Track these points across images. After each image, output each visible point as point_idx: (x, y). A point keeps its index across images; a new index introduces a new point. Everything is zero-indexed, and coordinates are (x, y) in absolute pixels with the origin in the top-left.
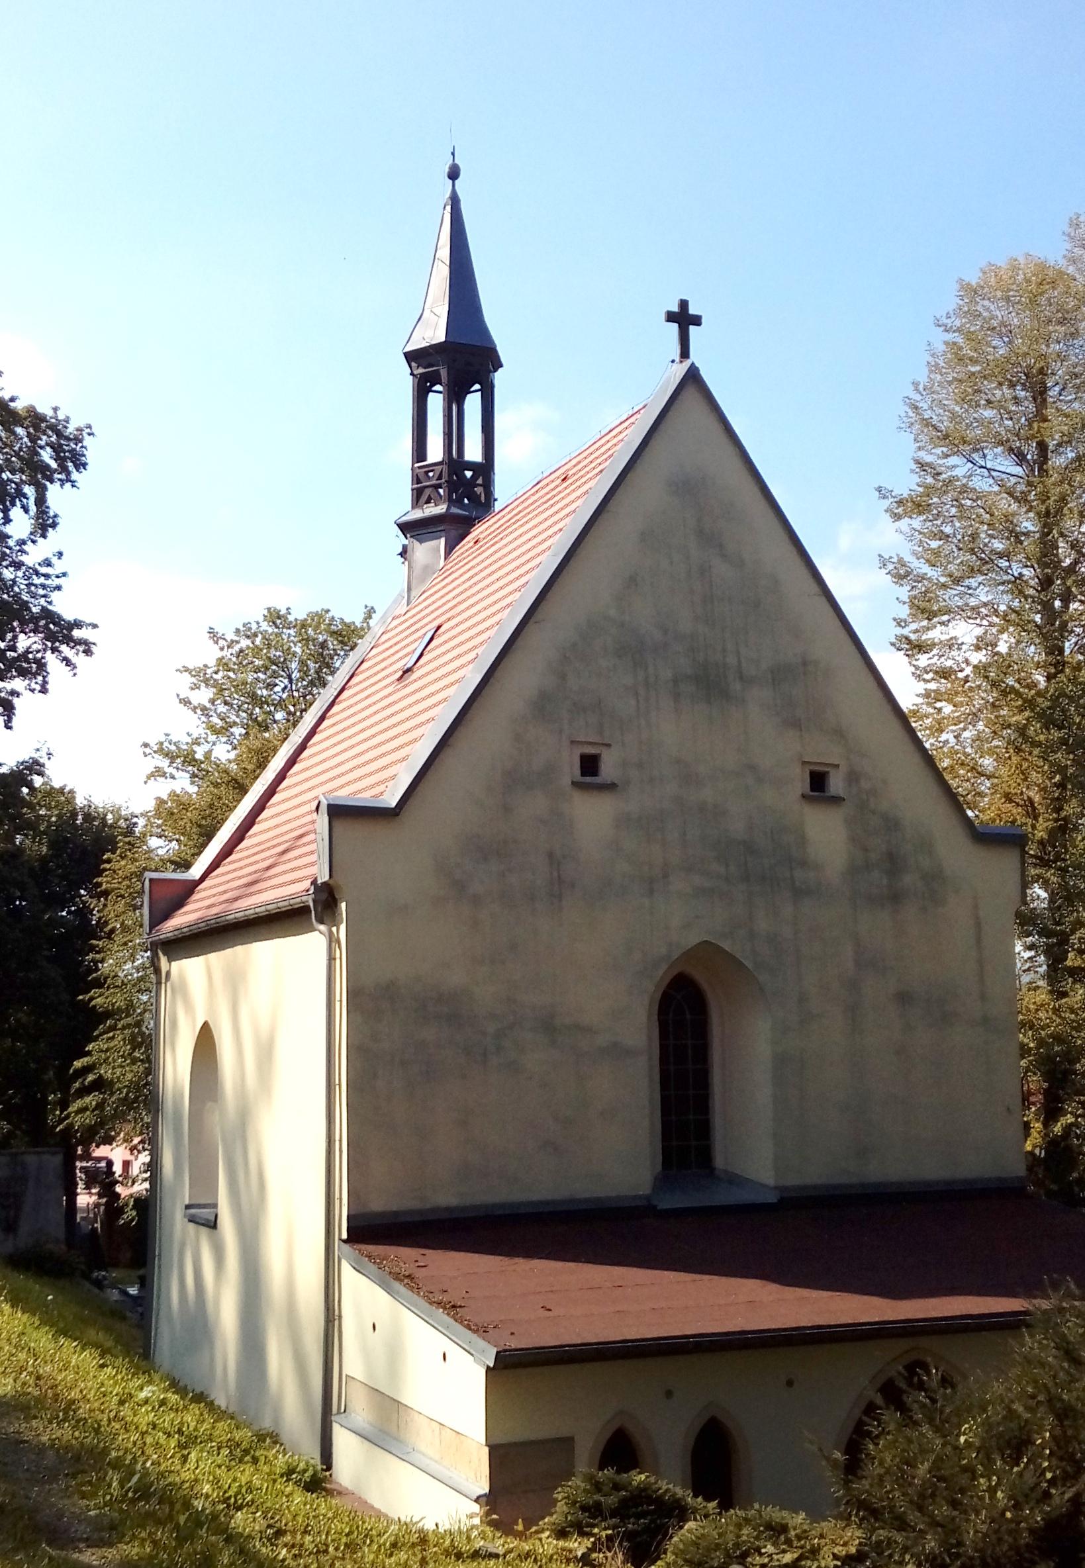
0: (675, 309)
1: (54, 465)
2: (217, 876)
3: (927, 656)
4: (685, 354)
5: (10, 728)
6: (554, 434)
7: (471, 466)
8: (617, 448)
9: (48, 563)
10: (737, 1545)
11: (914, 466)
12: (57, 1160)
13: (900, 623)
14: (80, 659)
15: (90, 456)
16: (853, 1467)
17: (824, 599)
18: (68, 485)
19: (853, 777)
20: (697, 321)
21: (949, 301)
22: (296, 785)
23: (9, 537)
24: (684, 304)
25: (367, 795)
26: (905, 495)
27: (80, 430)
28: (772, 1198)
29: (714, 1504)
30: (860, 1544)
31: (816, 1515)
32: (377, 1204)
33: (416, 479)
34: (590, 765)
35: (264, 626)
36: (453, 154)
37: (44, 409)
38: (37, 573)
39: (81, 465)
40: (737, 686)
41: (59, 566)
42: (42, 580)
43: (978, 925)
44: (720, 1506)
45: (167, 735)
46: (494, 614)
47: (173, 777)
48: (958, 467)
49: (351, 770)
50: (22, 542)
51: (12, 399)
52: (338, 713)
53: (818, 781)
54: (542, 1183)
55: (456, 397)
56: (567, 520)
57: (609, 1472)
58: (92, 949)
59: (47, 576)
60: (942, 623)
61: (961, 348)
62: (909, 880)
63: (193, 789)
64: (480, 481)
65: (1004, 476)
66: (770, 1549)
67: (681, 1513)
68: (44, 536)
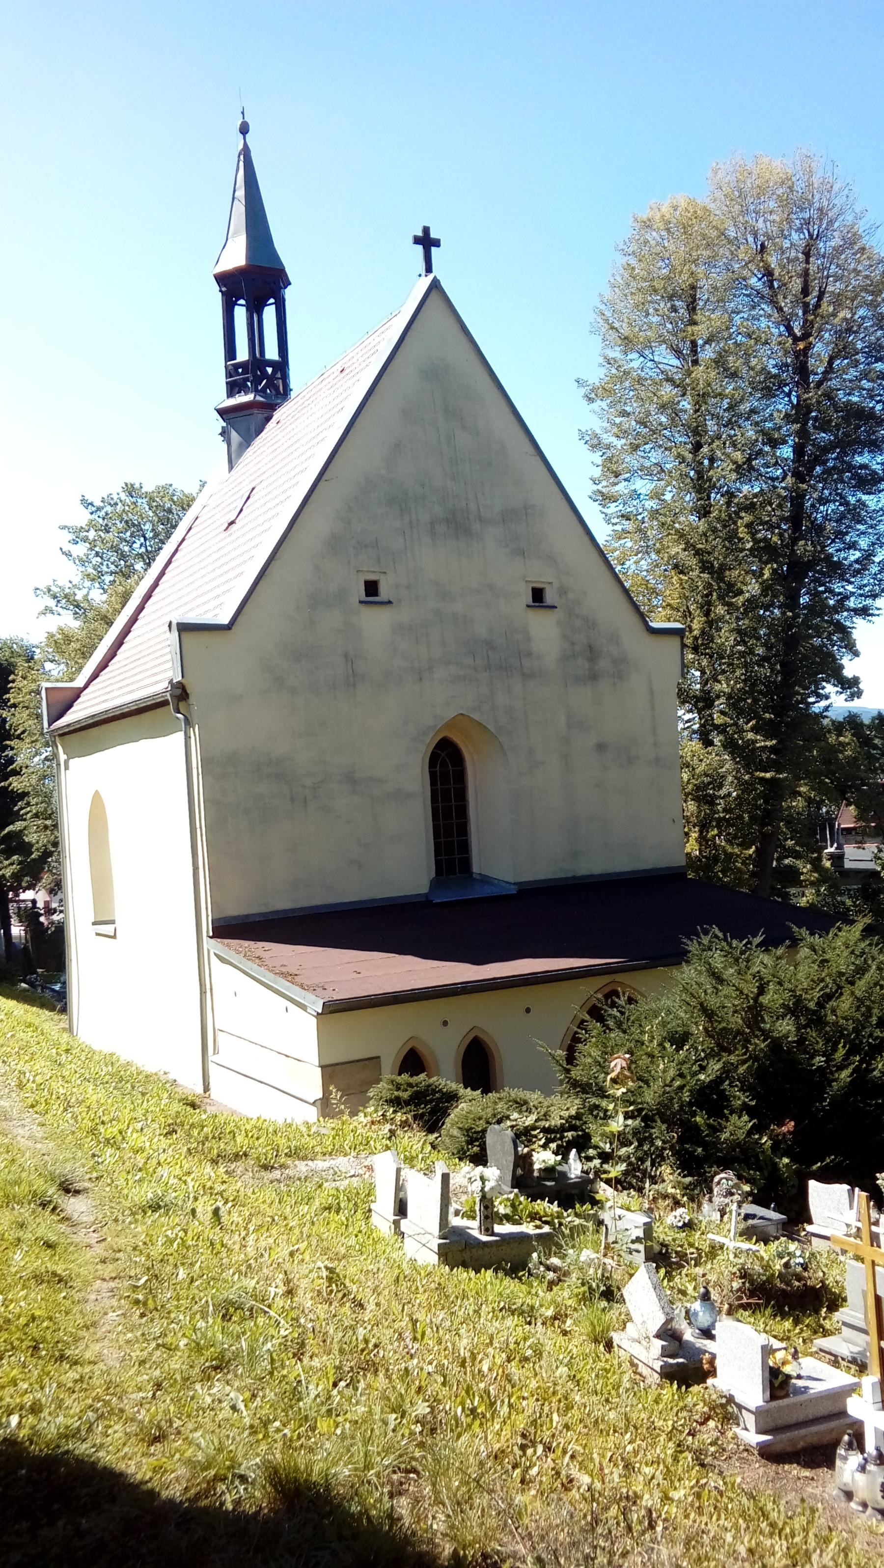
0: (420, 233)
3: (615, 504)
4: (429, 269)
7: (271, 363)
10: (494, 1115)
11: (601, 360)
13: (595, 481)
16: (571, 1059)
17: (538, 458)
19: (563, 591)
20: (437, 243)
21: (626, 230)
24: (426, 230)
26: (597, 384)
28: (513, 890)
29: (479, 1092)
31: (548, 1093)
32: (235, 909)
33: (229, 374)
34: (372, 588)
35: (123, 496)
40: (476, 526)
43: (652, 693)
48: (635, 362)
53: (538, 595)
57: (405, 1077)
60: (625, 480)
61: (633, 269)
62: (603, 664)
64: (279, 375)
65: (668, 367)
66: (515, 1115)
67: (452, 1098)
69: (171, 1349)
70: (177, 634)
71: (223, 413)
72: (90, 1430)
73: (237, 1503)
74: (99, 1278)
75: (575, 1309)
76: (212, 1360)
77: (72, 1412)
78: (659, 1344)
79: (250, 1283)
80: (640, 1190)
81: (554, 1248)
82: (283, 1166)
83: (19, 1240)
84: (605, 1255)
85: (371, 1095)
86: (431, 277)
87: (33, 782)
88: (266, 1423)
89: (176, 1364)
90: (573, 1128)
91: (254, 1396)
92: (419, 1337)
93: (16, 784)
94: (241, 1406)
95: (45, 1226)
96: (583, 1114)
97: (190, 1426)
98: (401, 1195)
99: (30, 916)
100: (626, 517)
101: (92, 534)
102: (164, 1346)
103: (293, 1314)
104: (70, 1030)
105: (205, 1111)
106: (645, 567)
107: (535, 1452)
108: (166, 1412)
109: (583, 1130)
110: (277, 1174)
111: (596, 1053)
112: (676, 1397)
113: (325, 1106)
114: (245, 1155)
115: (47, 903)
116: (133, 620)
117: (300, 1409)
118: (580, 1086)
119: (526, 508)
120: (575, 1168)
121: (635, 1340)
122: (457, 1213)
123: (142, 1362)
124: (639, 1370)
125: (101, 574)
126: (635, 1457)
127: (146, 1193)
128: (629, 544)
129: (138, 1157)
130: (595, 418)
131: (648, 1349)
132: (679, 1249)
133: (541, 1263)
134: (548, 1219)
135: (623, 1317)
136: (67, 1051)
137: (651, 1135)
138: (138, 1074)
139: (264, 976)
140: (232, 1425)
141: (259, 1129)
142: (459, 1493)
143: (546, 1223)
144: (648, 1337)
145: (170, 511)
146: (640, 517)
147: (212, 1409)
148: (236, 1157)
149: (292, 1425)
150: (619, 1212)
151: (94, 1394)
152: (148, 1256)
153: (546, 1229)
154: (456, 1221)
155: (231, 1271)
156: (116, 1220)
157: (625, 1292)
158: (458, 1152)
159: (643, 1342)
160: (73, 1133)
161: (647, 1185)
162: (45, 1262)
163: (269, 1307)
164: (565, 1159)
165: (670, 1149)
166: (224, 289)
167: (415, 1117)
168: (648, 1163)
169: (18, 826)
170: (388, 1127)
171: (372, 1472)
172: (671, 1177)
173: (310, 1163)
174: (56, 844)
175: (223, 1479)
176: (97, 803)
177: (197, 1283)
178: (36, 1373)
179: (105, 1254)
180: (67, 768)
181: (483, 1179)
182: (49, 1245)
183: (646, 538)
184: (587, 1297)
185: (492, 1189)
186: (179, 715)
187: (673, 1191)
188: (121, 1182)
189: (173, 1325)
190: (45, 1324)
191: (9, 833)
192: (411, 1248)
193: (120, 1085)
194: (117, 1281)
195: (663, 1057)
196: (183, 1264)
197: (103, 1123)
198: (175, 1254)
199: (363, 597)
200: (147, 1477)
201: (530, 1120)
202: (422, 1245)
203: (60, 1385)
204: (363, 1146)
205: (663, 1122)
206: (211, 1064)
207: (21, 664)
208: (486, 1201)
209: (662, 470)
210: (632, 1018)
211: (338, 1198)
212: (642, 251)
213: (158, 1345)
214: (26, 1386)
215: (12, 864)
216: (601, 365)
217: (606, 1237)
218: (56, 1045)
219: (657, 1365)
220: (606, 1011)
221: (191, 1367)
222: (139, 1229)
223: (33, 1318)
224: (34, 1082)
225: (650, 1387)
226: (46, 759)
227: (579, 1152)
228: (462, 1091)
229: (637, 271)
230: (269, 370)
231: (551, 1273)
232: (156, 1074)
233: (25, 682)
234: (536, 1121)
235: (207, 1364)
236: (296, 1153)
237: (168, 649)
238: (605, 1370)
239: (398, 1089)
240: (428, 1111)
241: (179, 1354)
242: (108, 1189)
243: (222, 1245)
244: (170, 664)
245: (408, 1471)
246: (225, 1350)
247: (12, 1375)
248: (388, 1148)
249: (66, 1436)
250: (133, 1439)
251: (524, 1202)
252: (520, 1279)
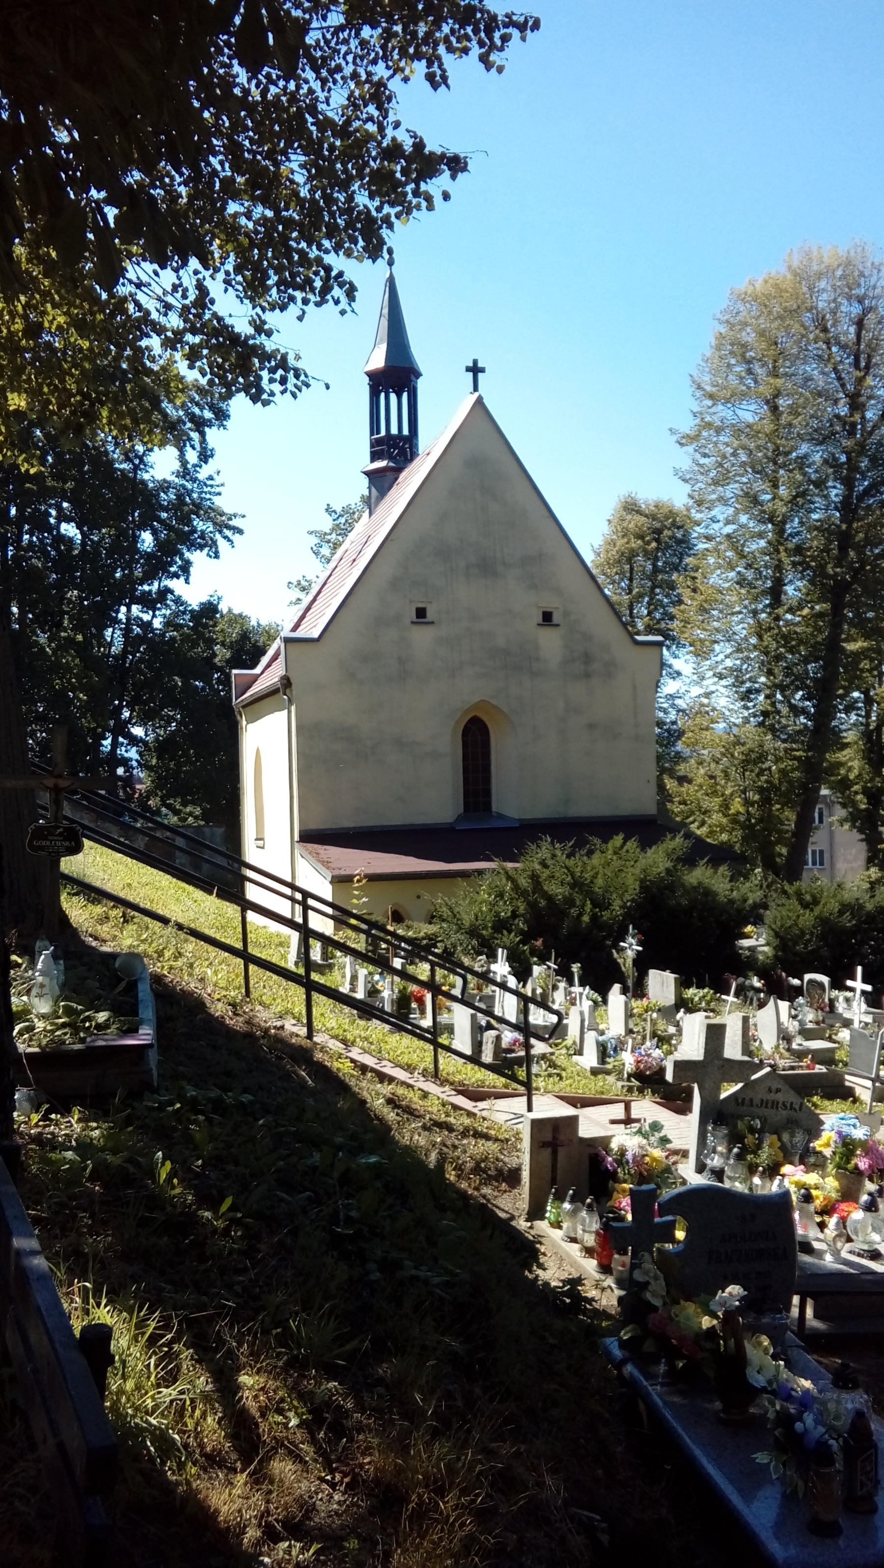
0: (471, 365)
4: (476, 389)
6: (439, 421)
9: (211, 478)
14: (236, 538)
19: (566, 614)
20: (482, 370)
24: (475, 362)
32: (313, 826)
33: (372, 446)
34: (421, 613)
38: (206, 486)
43: (635, 688)
50: (195, 466)
53: (547, 617)
59: (212, 486)
71: (367, 474)
86: (476, 394)
199: (415, 619)
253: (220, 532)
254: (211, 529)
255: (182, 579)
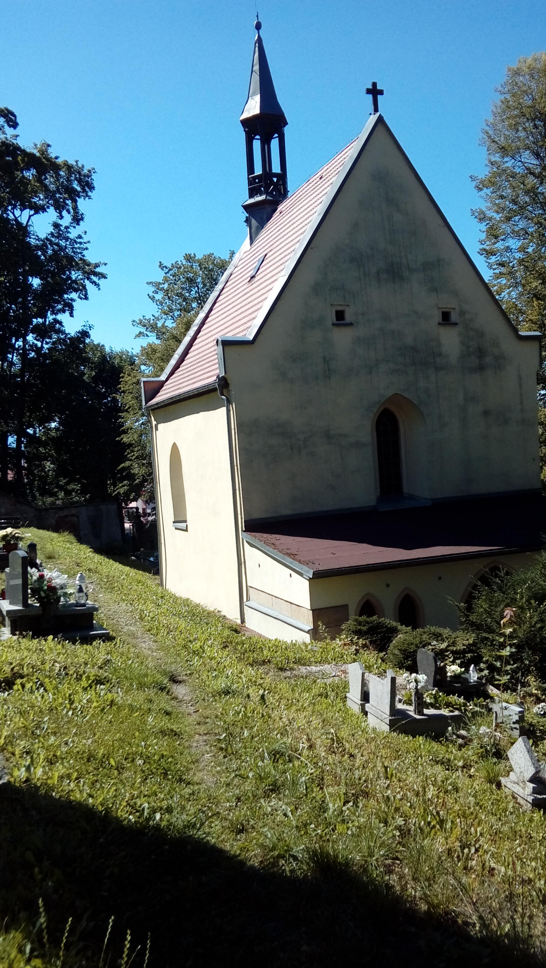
0: (370, 87)
1: (79, 189)
2: (173, 378)
4: (376, 110)
5: (73, 316)
7: (276, 175)
8: (345, 160)
9: (80, 237)
10: (421, 642)
11: (487, 162)
12: (114, 507)
13: (481, 242)
14: (102, 282)
15: (95, 184)
16: (469, 609)
18: (87, 198)
19: (462, 313)
20: (381, 92)
22: (202, 342)
23: (61, 226)
24: (374, 84)
25: (240, 335)
26: (484, 178)
27: (89, 171)
29: (410, 628)
30: (474, 640)
31: (454, 630)
32: (257, 515)
34: (340, 315)
35: (184, 262)
36: (257, 16)
37: (72, 162)
39: (92, 188)
41: (85, 239)
42: (78, 245)
43: (520, 378)
44: (412, 628)
45: (143, 316)
46: (296, 237)
47: (147, 336)
48: (509, 163)
49: (230, 326)
50: (67, 228)
51: (57, 158)
52: (222, 300)
54: (329, 503)
55: (266, 143)
56: (329, 188)
57: (363, 618)
58: (120, 417)
59: (81, 243)
60: (502, 240)
61: (508, 102)
63: (158, 342)
66: (435, 643)
67: (394, 631)
68: (78, 224)
69: (244, 778)
70: (221, 347)
71: (247, 208)
72: (202, 824)
73: (292, 871)
74: (197, 733)
75: (476, 762)
76: (269, 786)
77: (190, 812)
78: (531, 785)
79: (289, 740)
80: (515, 690)
81: (462, 725)
82: (292, 669)
83: (150, 709)
84: (496, 730)
85: (344, 628)
86: (378, 114)
87: (135, 437)
88: (306, 825)
89: (248, 786)
90: (470, 651)
91: (296, 809)
92: (389, 777)
93: (125, 439)
94: (290, 814)
95: (162, 702)
96: (477, 643)
97: (260, 824)
98: (365, 688)
99: (135, 516)
100: (502, 265)
101: (166, 286)
102: (240, 776)
103: (315, 760)
104: (161, 584)
105: (244, 635)
106: (514, 296)
107: (470, 851)
108: (245, 815)
109: (477, 653)
110: (288, 673)
111: (486, 606)
112: (543, 819)
113: (314, 633)
114: (269, 661)
115: (144, 510)
116: (194, 338)
117: (326, 818)
118: (476, 625)
119: (439, 260)
120: (473, 676)
121: (515, 783)
122: (400, 701)
123: (228, 785)
124: (518, 801)
125: (171, 310)
126: (523, 854)
127: (221, 683)
128: (504, 282)
129: (213, 662)
130: (482, 201)
131: (524, 789)
132: (542, 728)
133: (454, 733)
134: (458, 707)
135: (507, 768)
136: (162, 597)
137: (522, 657)
138: (203, 612)
139: (276, 556)
140: (284, 825)
141: (277, 645)
142: (428, 874)
143: (456, 709)
144: (524, 781)
145: (212, 270)
146: (511, 264)
147: (272, 815)
148: (264, 663)
149: (321, 827)
150: (505, 704)
151: (201, 802)
152: (225, 722)
153: (457, 713)
154: (399, 706)
155: (275, 732)
156: (204, 700)
157: (509, 753)
158: (398, 664)
159: (521, 784)
160: (174, 647)
161: (519, 687)
162: (165, 723)
163: (300, 755)
164: (467, 671)
165: (534, 666)
166: (246, 129)
167: (371, 642)
168: (520, 674)
169: (127, 463)
170: (354, 647)
171: (374, 858)
172: (535, 683)
173: (308, 668)
174: (151, 474)
175: (283, 857)
176: (175, 450)
177: (256, 739)
178: (167, 788)
179: (199, 719)
180: (157, 429)
181: (416, 681)
182: (168, 713)
183: (515, 278)
184: (484, 755)
185: (422, 687)
186: (223, 397)
187: (536, 692)
188: (204, 677)
189: (244, 764)
190: (170, 760)
191: (122, 468)
192: (372, 721)
193: (193, 618)
194: (208, 735)
195: (529, 609)
196: (246, 727)
197: (190, 641)
198: (241, 721)
200: (238, 853)
201: (443, 646)
202: (378, 718)
203: (181, 796)
204: (339, 659)
205: (530, 649)
206: (245, 607)
207: (128, 368)
208: (419, 694)
209: (526, 233)
210: (509, 584)
211: (326, 689)
212: (515, 90)
213: (236, 775)
214: (162, 796)
215: (123, 486)
216: (486, 165)
217: (496, 719)
218: (156, 594)
219: (530, 799)
220: (491, 579)
221: (257, 789)
222: (218, 705)
223: (163, 756)
224: (149, 616)
225: (526, 812)
226: (142, 424)
227: (475, 666)
228: (399, 627)
229: (511, 103)
230: (275, 180)
231: (461, 740)
232: (213, 612)
233: (130, 378)
234: (447, 646)
235: (266, 788)
236: (300, 662)
237: (216, 356)
238: (497, 800)
239: (360, 625)
240: (378, 639)
241: (249, 781)
242: (197, 681)
243: (269, 717)
244: (217, 366)
245: (393, 859)
246: (277, 780)
247: (154, 789)
248: (355, 661)
249: (189, 827)
250: (227, 831)
251: (442, 696)
252: (441, 742)
253: (88, 279)
254: (81, 277)
255: (67, 313)
